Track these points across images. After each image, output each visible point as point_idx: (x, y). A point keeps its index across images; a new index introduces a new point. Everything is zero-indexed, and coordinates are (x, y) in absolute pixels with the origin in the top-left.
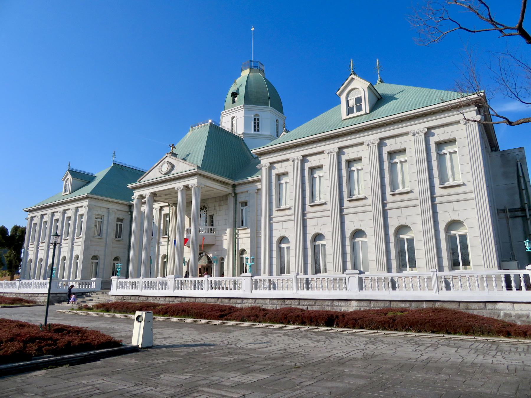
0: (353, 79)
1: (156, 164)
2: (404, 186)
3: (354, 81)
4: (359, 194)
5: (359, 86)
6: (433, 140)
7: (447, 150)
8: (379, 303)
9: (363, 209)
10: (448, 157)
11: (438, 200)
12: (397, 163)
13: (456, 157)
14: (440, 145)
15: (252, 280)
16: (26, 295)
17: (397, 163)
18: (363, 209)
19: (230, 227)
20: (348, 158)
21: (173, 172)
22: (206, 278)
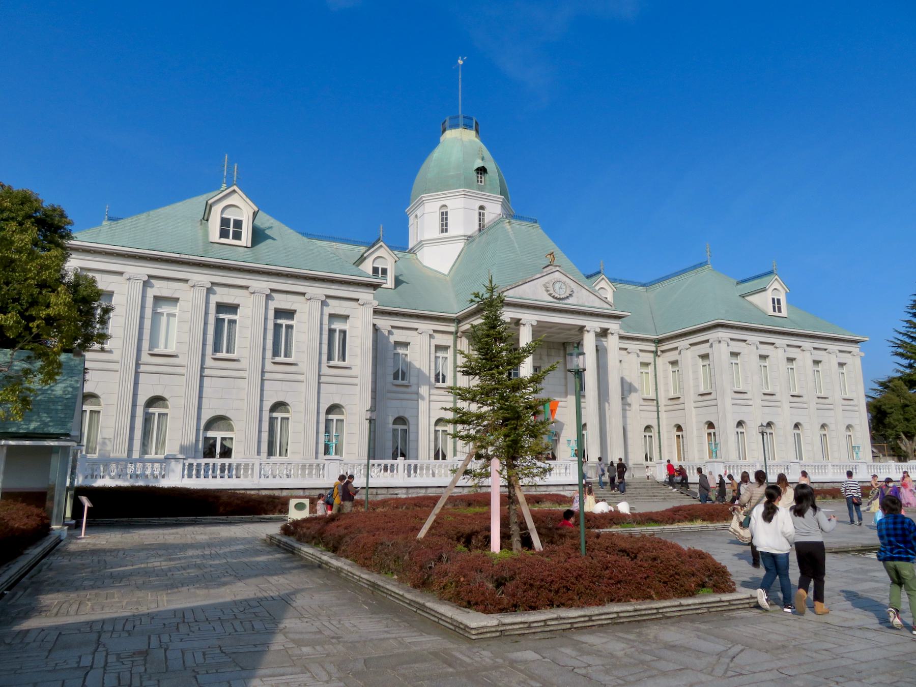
0: (234, 191)
1: (538, 276)
2: (166, 347)
3: (235, 196)
4: (166, 347)
5: (243, 209)
6: (151, 293)
7: (164, 309)
8: (418, 490)
9: (800, 405)
10: (164, 319)
11: (143, 368)
12: (162, 314)
13: (174, 322)
14: (158, 299)
15: (184, 464)
16: (567, 488)
17: (162, 314)
18: (800, 405)
19: (572, 394)
20: (220, 300)
21: (570, 301)
22: (400, 461)
